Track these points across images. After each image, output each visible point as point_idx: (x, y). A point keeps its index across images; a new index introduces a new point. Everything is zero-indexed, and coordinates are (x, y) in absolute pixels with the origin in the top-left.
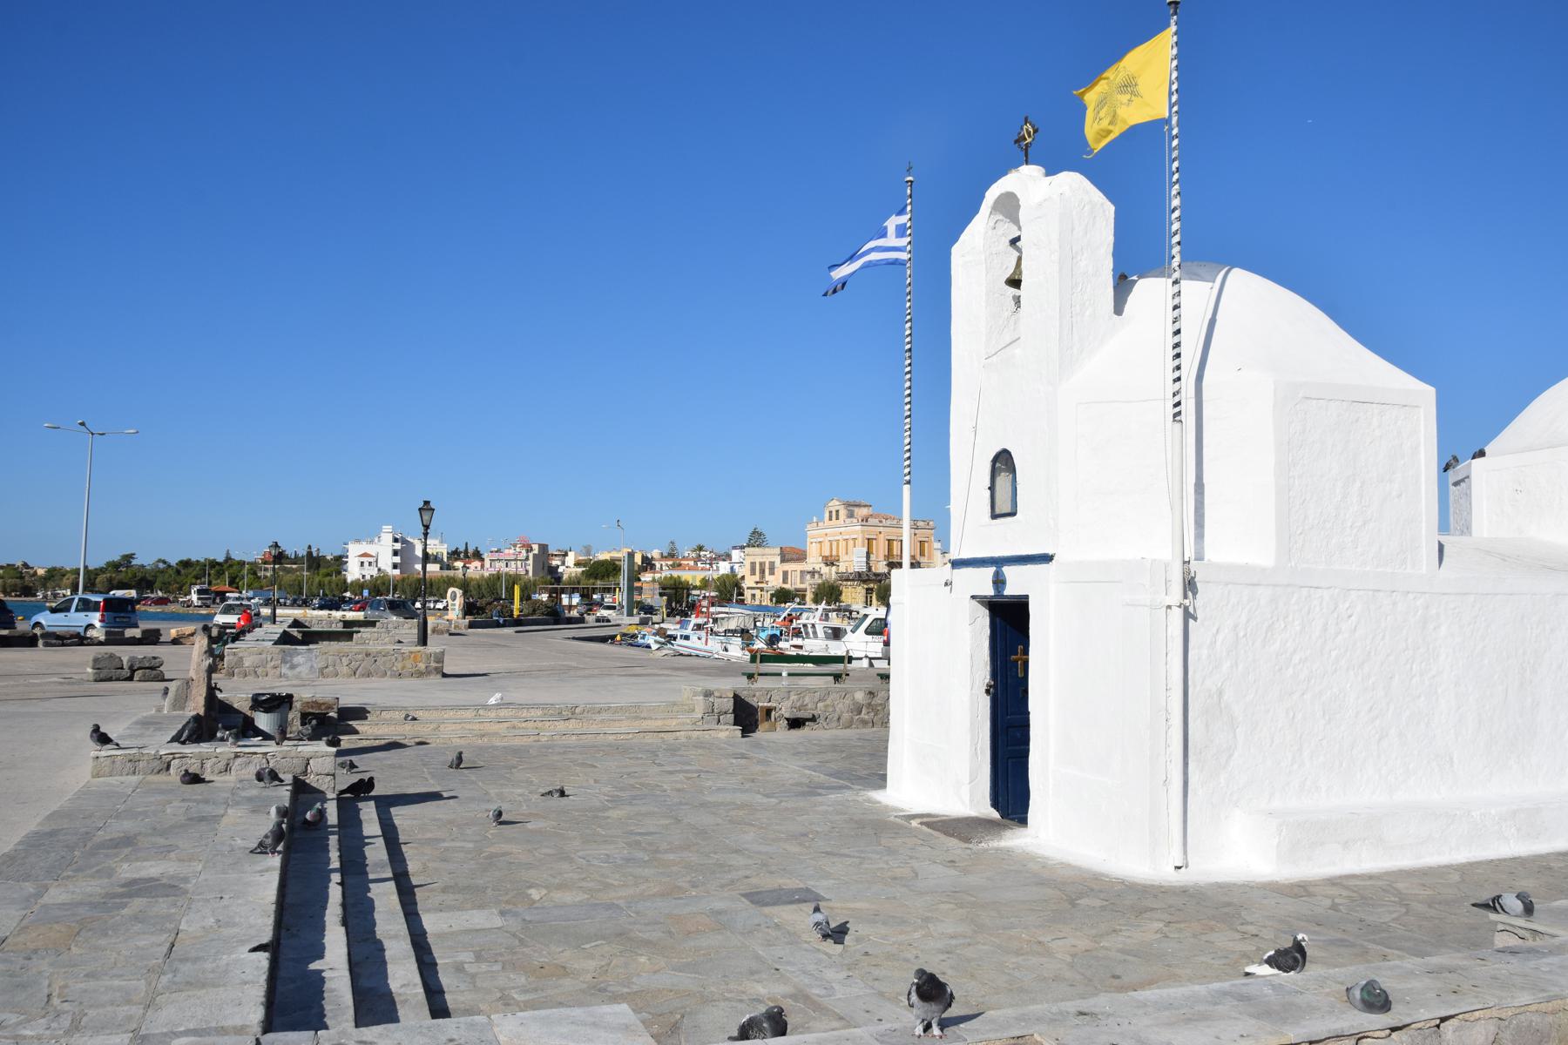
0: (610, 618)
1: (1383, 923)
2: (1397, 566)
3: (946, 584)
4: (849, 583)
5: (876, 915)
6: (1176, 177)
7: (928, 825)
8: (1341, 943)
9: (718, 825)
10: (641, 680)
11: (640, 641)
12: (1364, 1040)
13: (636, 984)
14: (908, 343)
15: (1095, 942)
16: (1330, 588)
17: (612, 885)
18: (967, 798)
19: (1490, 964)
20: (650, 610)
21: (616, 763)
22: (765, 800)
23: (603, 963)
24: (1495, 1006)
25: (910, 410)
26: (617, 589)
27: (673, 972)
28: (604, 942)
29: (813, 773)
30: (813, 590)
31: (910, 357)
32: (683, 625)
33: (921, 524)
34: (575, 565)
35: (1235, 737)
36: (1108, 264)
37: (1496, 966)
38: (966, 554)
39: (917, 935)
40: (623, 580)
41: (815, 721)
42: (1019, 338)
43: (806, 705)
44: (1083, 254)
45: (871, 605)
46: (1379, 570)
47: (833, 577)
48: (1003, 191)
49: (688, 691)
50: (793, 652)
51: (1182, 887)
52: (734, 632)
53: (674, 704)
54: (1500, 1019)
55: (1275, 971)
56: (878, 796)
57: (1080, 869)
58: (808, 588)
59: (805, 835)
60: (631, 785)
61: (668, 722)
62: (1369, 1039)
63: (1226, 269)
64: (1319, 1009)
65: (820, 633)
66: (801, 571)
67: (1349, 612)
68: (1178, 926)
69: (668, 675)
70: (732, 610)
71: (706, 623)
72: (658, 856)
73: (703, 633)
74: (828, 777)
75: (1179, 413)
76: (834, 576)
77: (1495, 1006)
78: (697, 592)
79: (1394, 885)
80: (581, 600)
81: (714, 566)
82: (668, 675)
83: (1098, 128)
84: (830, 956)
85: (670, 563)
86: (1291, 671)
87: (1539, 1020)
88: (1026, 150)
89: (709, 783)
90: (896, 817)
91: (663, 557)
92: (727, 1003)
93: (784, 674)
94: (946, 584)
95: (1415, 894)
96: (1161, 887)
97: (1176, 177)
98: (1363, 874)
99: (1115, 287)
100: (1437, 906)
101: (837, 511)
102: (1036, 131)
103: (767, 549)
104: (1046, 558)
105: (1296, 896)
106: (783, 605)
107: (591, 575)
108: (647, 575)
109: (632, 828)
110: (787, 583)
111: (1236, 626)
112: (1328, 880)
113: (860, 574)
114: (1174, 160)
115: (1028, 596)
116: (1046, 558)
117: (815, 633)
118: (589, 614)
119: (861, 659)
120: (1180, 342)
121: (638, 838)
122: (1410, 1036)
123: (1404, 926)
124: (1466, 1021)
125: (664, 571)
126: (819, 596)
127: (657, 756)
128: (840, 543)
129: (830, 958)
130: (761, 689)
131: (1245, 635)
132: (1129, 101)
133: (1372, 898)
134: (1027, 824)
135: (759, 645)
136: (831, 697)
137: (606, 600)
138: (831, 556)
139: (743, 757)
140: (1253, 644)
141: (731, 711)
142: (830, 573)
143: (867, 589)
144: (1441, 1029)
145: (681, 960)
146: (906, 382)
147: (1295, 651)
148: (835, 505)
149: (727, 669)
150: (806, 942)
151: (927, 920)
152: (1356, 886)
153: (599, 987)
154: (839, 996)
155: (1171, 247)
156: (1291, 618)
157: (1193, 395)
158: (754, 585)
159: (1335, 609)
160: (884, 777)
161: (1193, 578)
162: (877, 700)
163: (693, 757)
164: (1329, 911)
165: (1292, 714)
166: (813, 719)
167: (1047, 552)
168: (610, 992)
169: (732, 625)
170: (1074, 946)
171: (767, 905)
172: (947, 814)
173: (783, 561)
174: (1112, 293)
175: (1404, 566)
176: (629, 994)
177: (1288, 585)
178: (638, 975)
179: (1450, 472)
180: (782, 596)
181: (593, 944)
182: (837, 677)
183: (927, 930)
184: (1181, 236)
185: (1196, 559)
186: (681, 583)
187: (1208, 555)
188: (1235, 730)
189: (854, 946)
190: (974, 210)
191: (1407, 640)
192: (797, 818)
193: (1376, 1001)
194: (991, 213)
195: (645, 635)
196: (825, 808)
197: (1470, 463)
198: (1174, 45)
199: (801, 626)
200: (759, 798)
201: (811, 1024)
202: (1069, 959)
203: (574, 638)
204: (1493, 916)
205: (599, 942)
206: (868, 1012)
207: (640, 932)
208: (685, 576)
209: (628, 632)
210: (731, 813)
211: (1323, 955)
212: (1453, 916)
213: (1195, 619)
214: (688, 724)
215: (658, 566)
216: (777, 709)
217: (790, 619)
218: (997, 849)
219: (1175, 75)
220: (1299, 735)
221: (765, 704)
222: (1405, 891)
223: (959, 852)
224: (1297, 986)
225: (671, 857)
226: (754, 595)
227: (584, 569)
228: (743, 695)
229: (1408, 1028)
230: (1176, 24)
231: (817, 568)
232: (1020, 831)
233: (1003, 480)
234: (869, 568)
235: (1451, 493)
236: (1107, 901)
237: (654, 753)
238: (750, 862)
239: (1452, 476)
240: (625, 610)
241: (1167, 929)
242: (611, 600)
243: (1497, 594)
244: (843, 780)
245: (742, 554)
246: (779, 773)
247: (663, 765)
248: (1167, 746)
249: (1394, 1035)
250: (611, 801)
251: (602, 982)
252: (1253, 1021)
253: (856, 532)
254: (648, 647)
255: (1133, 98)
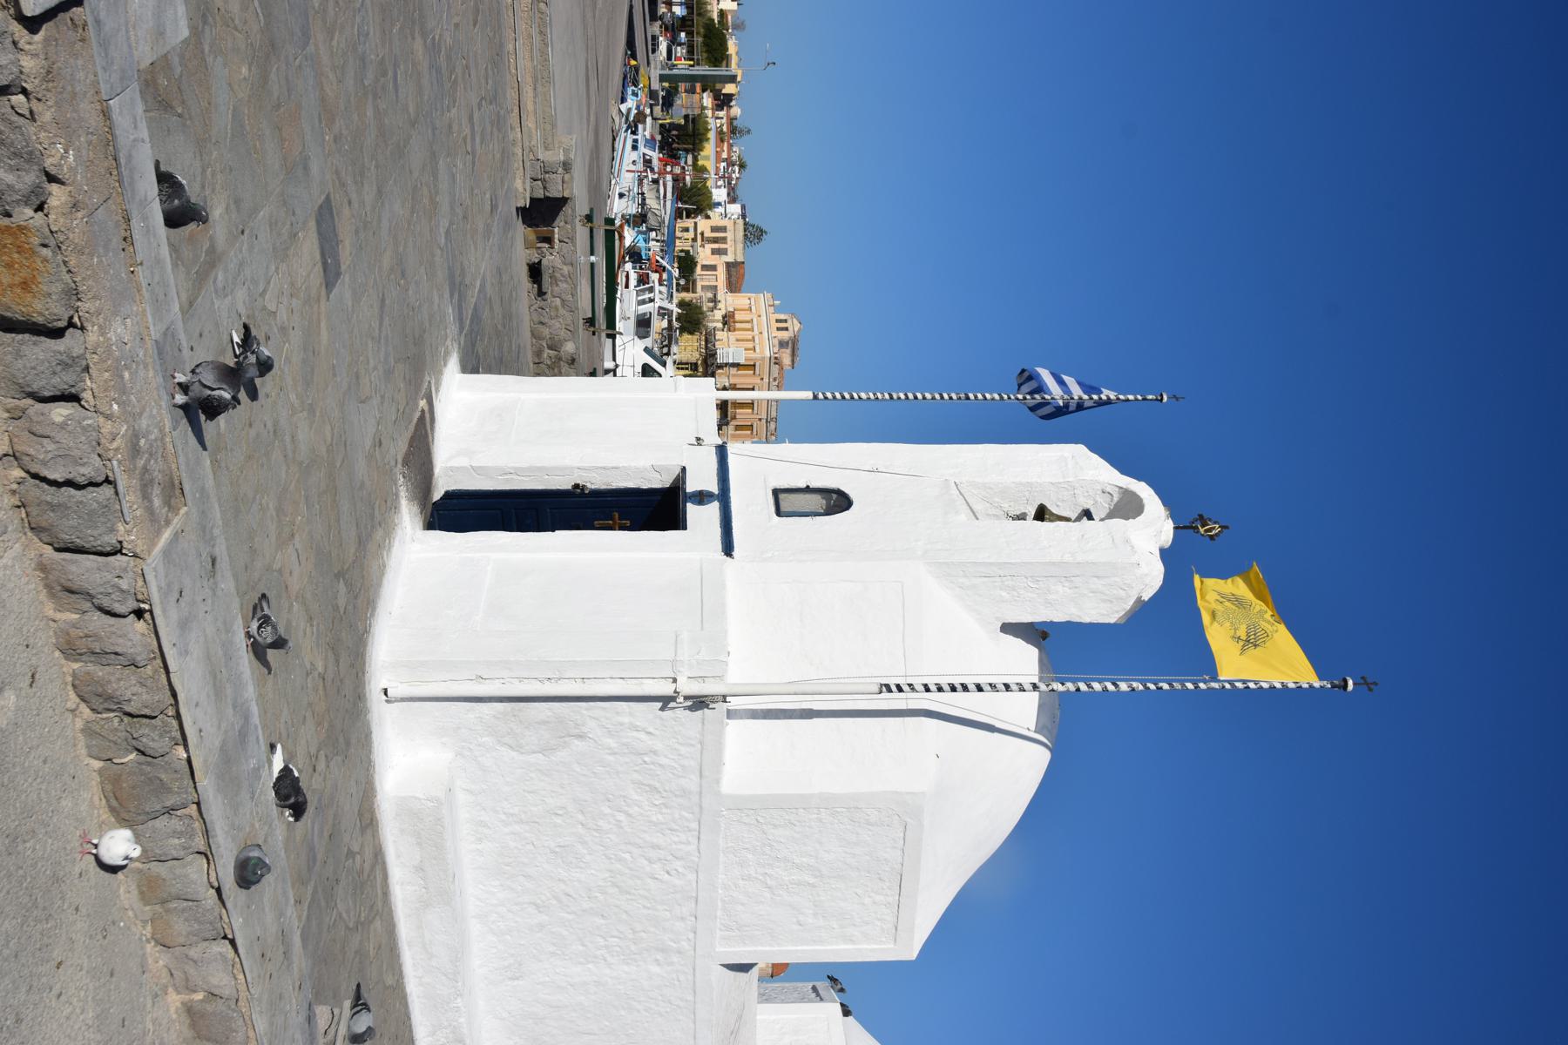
0: (657, 53)
1: (336, 904)
2: (723, 921)
3: (698, 439)
4: (703, 343)
5: (314, 353)
6: (1152, 687)
7: (422, 418)
8: (312, 859)
9: (411, 172)
10: (582, 87)
11: (630, 90)
12: (205, 861)
13: (214, 61)
14: (976, 397)
15: (297, 597)
16: (699, 853)
17: (332, 39)
18: (456, 463)
19: (296, 994)
20: (668, 103)
21: (479, 52)
22: (442, 231)
23: (237, 22)
24: (251, 995)
25: (899, 398)
26: (692, 63)
27: (231, 107)
28: (262, 25)
29: (477, 290)
30: (694, 301)
31: (959, 398)
32: (650, 142)
33: (772, 426)
34: (721, 10)
35: (534, 752)
36: (1058, 617)
37: (294, 1000)
38: (732, 461)
39: (293, 397)
40: (704, 70)
41: (539, 296)
42: (977, 519)
43: (557, 285)
44: (1070, 588)
45: (678, 368)
46: (720, 904)
47: (710, 324)
48: (1145, 501)
49: (570, 143)
50: (621, 279)
51: (365, 695)
52: (643, 204)
53: (554, 126)
54: (237, 1000)
55: (276, 774)
56: (453, 364)
57: (379, 585)
58: (698, 295)
59: (403, 275)
60: (454, 68)
61: (532, 118)
62: (206, 865)
63: (1049, 744)
64: (236, 815)
65: (643, 309)
66: (716, 286)
67: (673, 872)
68: (321, 688)
69: (588, 120)
70: (669, 204)
71: (652, 170)
72: (370, 97)
73: (640, 166)
74: (472, 307)
75: (890, 691)
76: (711, 325)
77: (251, 995)
78: (690, 161)
79: (378, 918)
80: (678, 17)
81: (720, 183)
82: (588, 120)
83: (1211, 592)
84: (263, 294)
85: (725, 129)
86: (608, 811)
87: (238, 1039)
88: (1191, 527)
89: (460, 165)
90: (429, 382)
91: (731, 120)
92: (200, 170)
93: (593, 258)
94: (698, 439)
95: (369, 938)
96: (364, 673)
97: (1152, 687)
98: (388, 887)
99: (1032, 624)
100: (357, 959)
101: (787, 329)
102: (1212, 537)
103: (742, 245)
104: (728, 549)
105: (360, 815)
106: (676, 265)
107: (709, 29)
108: (710, 100)
109: (402, 67)
110: (702, 270)
111: (655, 753)
112: (381, 849)
113: (714, 355)
114: (1170, 684)
116: (728, 549)
117: (643, 302)
118: (661, 27)
119: (614, 359)
120: (968, 691)
121: (390, 74)
122: (213, 909)
123: (334, 923)
124: (233, 966)
125: (715, 121)
126: (688, 308)
127: (491, 103)
128: (750, 333)
129: (260, 295)
130: (574, 229)
131: (645, 762)
132: (1239, 638)
133: (362, 893)
134: (428, 529)
135: (629, 236)
136: (567, 314)
137: (679, 48)
138: (734, 322)
139: (494, 208)
140: (635, 771)
141: (547, 194)
142: (715, 319)
143: (696, 364)
144: (223, 941)
145: (246, 118)
146: (931, 394)
147: (629, 815)
148: (794, 326)
149: (598, 191)
150: (277, 268)
151: (311, 410)
152: (375, 877)
153: (208, 15)
154: (217, 303)
155: (1074, 681)
156: (664, 810)
157: (910, 707)
158: (699, 231)
159: (677, 858)
160: (475, 371)
161: (707, 706)
162: (565, 367)
163: (491, 146)
164: (346, 849)
165: (560, 812)
166: (541, 293)
167: (735, 549)
168: (203, 27)
169: (651, 202)
170: (291, 573)
171: (319, 224)
172: (435, 441)
173: (728, 265)
174: (1026, 621)
175: (724, 929)
176: (203, 52)
177: (701, 807)
178: (225, 65)
179: (828, 983)
180: (687, 264)
181: (259, 11)
182: (591, 322)
183: (300, 409)
184: (1086, 692)
185: (728, 711)
186: (701, 141)
187: (734, 726)
188: (540, 752)
189: (276, 324)
190: (1124, 470)
191: (644, 931)
192: (423, 267)
193: (249, 873)
194: (1121, 488)
195: (637, 95)
196: (436, 301)
197: (836, 1002)
198: (1298, 685)
199: (651, 285)
200: (444, 223)
201: (181, 267)
202: (276, 566)
203: (631, 7)
204: (347, 1004)
205: (262, 18)
206: (201, 335)
207: (277, 69)
208: (709, 149)
209: (640, 76)
210: (425, 188)
211: (298, 838)
212: (347, 975)
213: (662, 709)
214: (530, 142)
215: (721, 114)
216: (551, 250)
217: (660, 269)
218: (397, 495)
219: (1265, 686)
220: (537, 820)
221: (556, 236)
222: (372, 927)
223: (392, 451)
224: (260, 795)
225: (370, 113)
226: (687, 230)
227: (716, 21)
228: (567, 209)
229: (221, 906)
230: (1321, 687)
231: (720, 305)
232: (418, 522)
233: (817, 502)
234: (721, 367)
235: (806, 984)
236: (345, 613)
237: (494, 99)
238: (368, 208)
239: (823, 985)
240: (667, 72)
241: (317, 675)
242: (679, 55)
243: (695, 1023)
244: (471, 326)
245: (736, 216)
246: (476, 249)
247: (479, 109)
248: (521, 679)
249: (213, 892)
250: (434, 44)
251: (214, 19)
252: (217, 743)
253: (762, 351)
254: (623, 100)
255: (1241, 643)
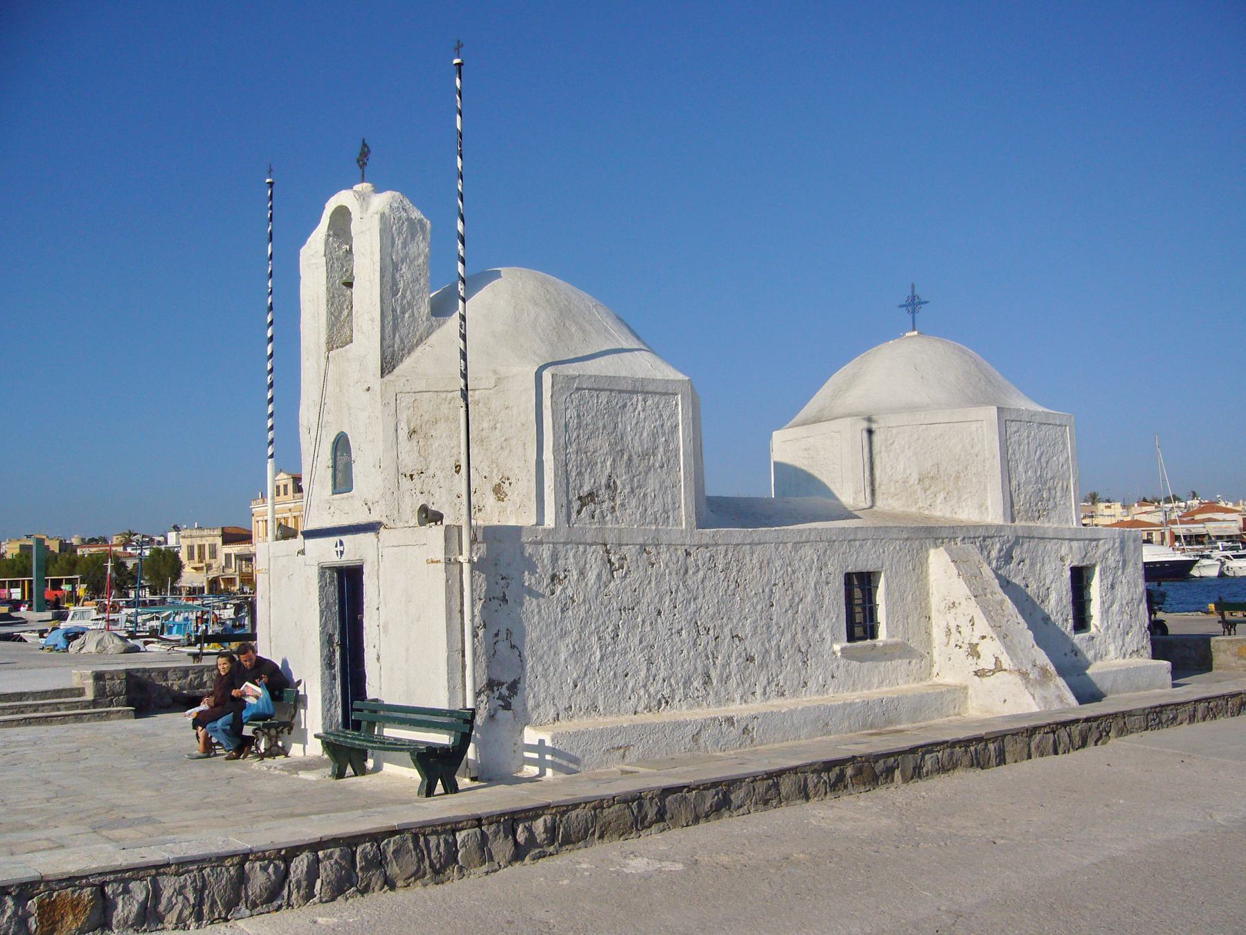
101: (286, 486)
115: (848, 577)
128: (289, 520)
173: (225, 542)
